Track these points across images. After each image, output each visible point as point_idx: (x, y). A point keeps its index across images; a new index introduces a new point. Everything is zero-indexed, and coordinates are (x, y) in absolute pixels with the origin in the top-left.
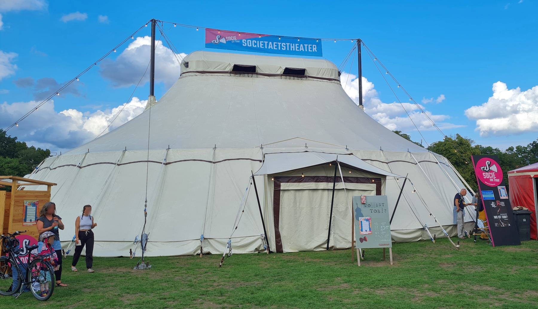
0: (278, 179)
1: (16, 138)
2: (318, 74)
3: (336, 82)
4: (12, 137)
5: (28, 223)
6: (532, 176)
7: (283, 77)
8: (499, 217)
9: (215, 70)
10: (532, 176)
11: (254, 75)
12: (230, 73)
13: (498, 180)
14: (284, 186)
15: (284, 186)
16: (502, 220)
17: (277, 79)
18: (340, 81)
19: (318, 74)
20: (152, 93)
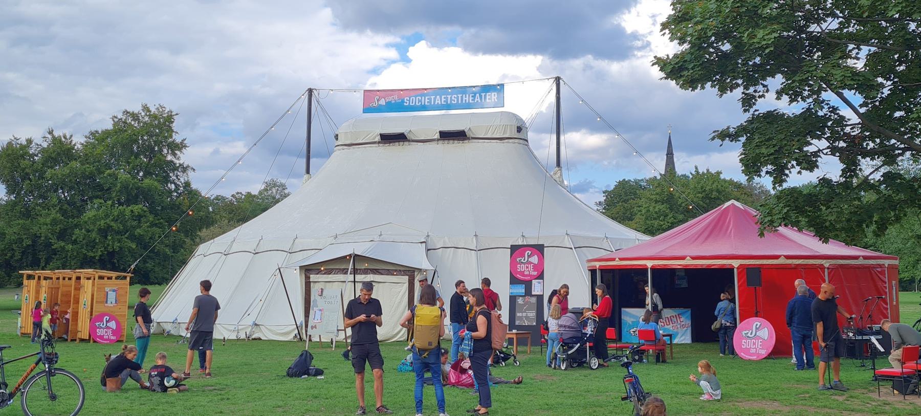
0: (308, 270)
1: (719, 173)
2: (486, 134)
3: (521, 141)
4: (713, 171)
5: (109, 304)
6: (827, 265)
7: (441, 142)
8: (524, 314)
9: (361, 142)
10: (827, 265)
11: (406, 143)
12: (379, 143)
13: (535, 273)
14: (313, 277)
15: (313, 277)
16: (527, 317)
17: (433, 145)
18: (527, 141)
19: (486, 134)
20: (308, 172)
